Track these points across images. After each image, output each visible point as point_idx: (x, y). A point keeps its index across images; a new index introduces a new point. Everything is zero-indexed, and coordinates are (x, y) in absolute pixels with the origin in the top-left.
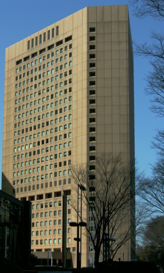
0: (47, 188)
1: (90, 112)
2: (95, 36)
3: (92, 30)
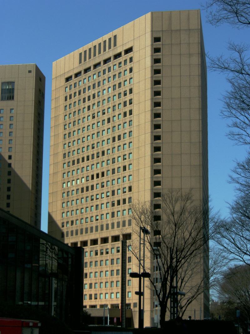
0: (102, 231)
2: (161, 135)
3: (157, 40)
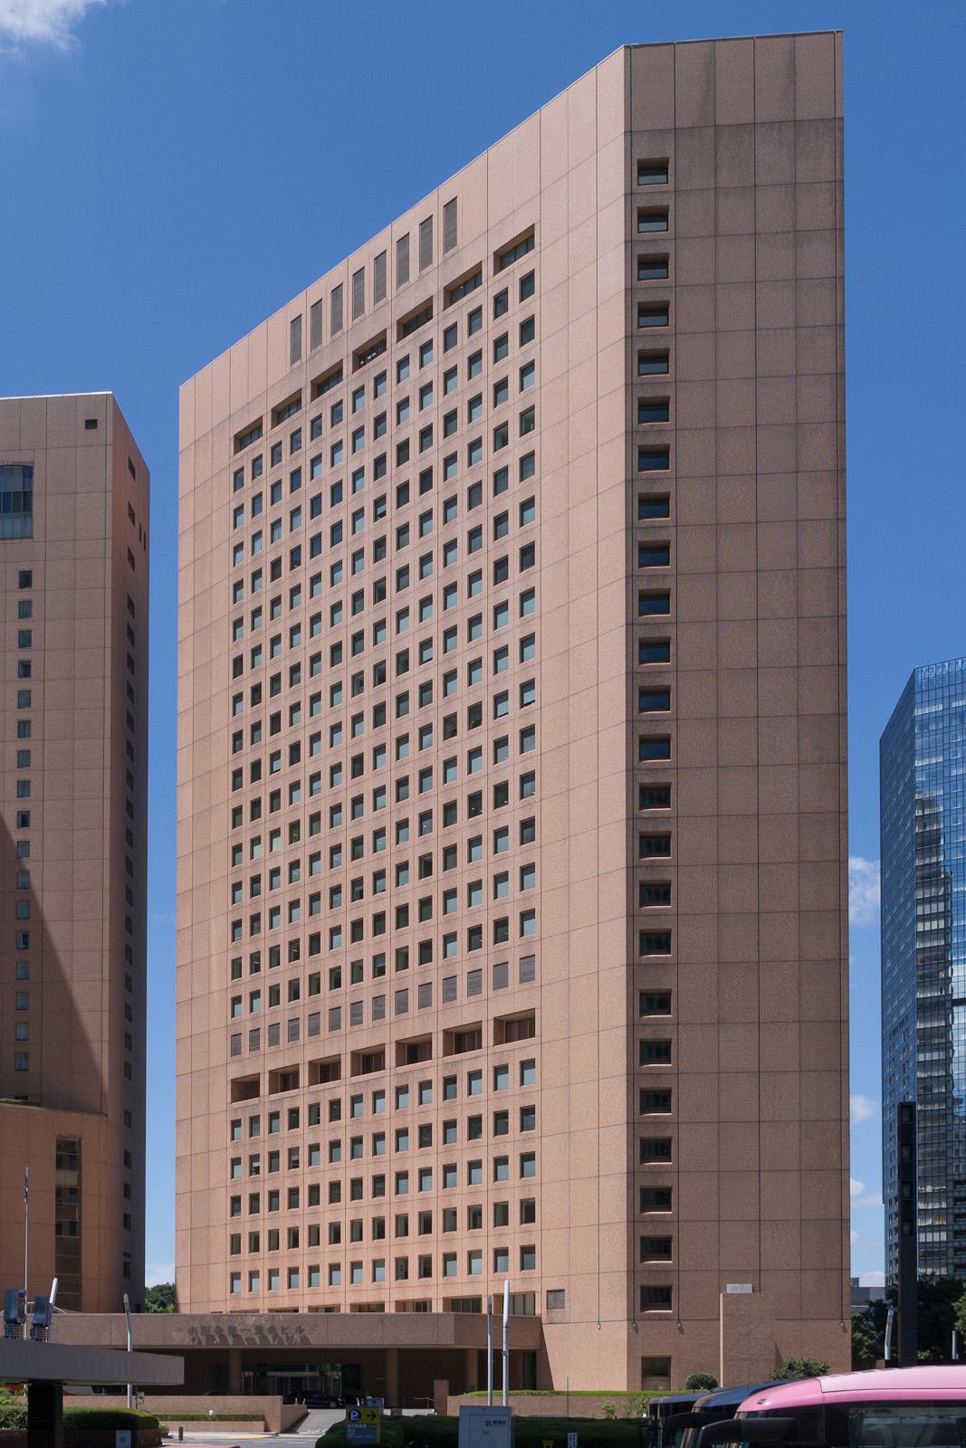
0: (404, 1015)
1: (645, 1256)
3: (647, 169)
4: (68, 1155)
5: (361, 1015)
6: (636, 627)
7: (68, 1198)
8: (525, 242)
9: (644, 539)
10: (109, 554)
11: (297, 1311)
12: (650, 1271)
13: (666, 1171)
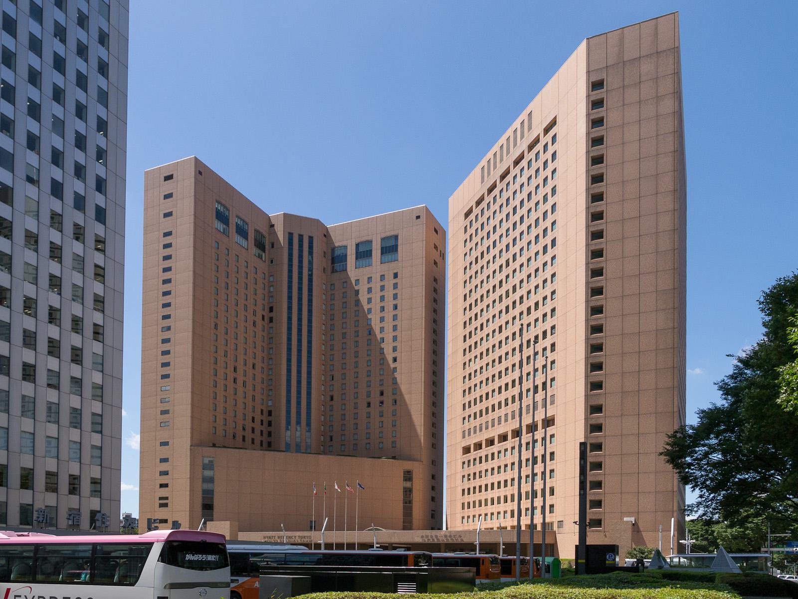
2: (601, 481)
3: (596, 85)
4: (408, 476)
5: (501, 421)
6: (590, 265)
7: (408, 492)
8: (553, 123)
9: (593, 230)
10: (424, 263)
11: (493, 529)
12: (593, 513)
13: (600, 474)
